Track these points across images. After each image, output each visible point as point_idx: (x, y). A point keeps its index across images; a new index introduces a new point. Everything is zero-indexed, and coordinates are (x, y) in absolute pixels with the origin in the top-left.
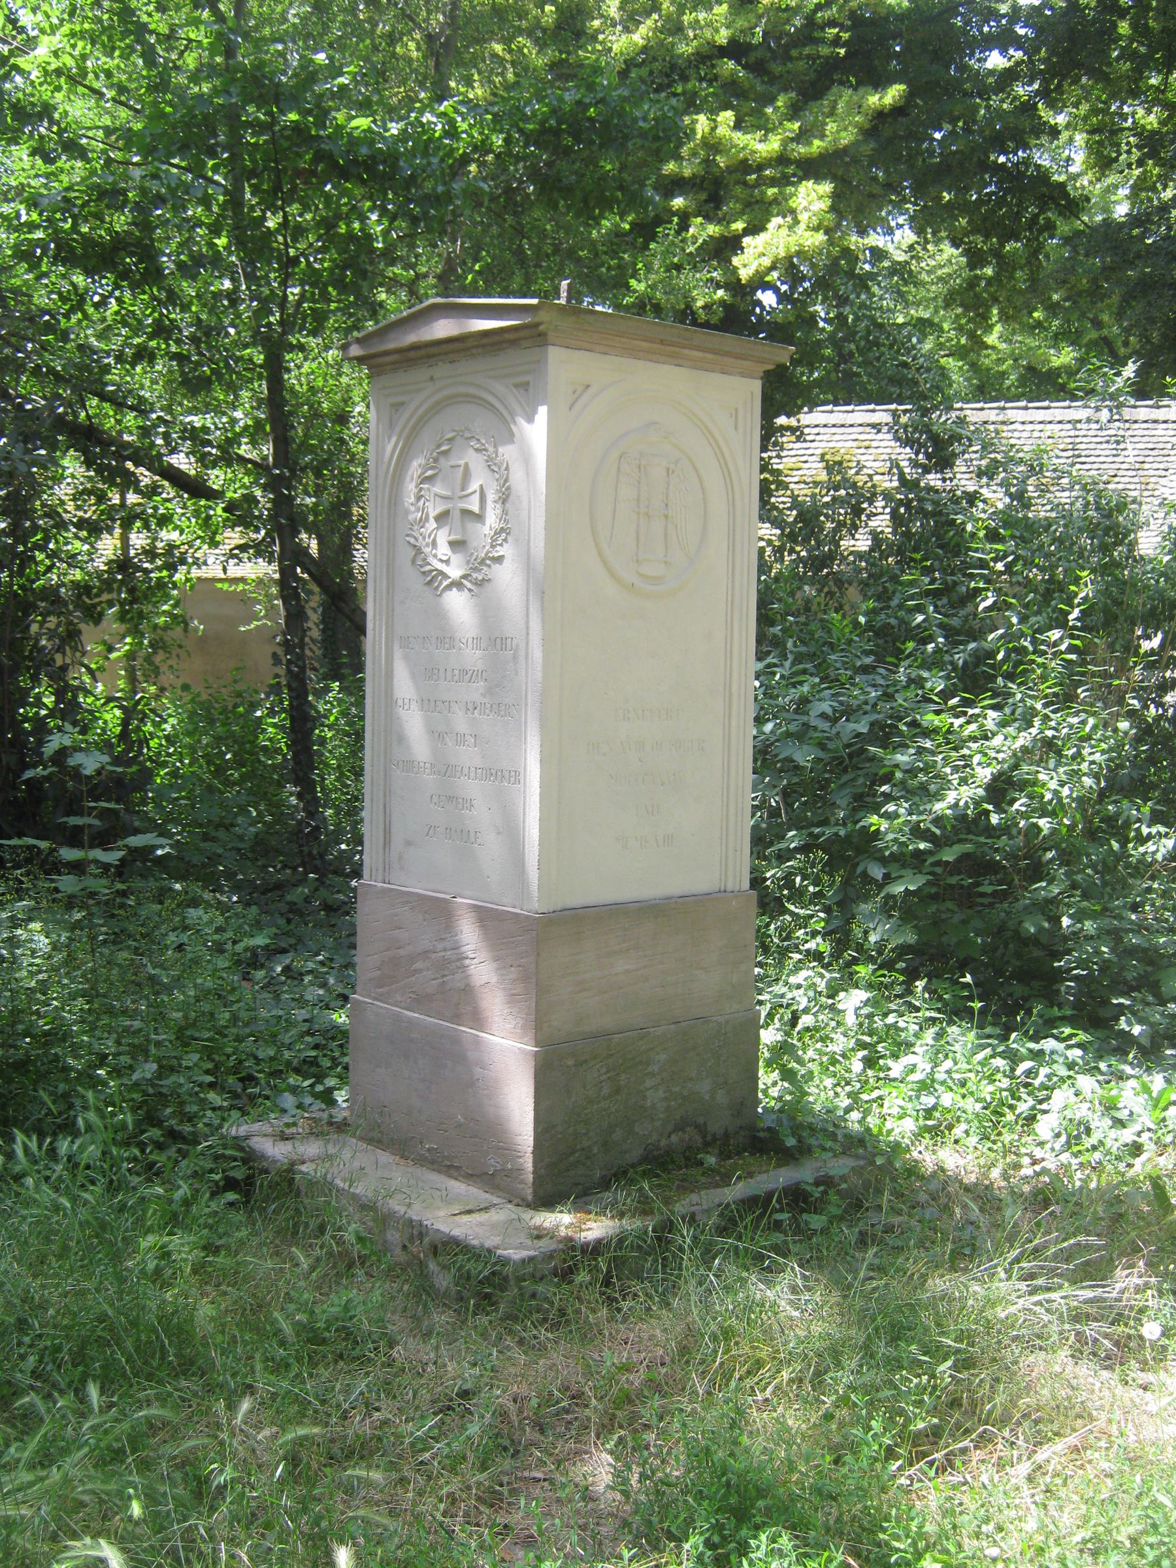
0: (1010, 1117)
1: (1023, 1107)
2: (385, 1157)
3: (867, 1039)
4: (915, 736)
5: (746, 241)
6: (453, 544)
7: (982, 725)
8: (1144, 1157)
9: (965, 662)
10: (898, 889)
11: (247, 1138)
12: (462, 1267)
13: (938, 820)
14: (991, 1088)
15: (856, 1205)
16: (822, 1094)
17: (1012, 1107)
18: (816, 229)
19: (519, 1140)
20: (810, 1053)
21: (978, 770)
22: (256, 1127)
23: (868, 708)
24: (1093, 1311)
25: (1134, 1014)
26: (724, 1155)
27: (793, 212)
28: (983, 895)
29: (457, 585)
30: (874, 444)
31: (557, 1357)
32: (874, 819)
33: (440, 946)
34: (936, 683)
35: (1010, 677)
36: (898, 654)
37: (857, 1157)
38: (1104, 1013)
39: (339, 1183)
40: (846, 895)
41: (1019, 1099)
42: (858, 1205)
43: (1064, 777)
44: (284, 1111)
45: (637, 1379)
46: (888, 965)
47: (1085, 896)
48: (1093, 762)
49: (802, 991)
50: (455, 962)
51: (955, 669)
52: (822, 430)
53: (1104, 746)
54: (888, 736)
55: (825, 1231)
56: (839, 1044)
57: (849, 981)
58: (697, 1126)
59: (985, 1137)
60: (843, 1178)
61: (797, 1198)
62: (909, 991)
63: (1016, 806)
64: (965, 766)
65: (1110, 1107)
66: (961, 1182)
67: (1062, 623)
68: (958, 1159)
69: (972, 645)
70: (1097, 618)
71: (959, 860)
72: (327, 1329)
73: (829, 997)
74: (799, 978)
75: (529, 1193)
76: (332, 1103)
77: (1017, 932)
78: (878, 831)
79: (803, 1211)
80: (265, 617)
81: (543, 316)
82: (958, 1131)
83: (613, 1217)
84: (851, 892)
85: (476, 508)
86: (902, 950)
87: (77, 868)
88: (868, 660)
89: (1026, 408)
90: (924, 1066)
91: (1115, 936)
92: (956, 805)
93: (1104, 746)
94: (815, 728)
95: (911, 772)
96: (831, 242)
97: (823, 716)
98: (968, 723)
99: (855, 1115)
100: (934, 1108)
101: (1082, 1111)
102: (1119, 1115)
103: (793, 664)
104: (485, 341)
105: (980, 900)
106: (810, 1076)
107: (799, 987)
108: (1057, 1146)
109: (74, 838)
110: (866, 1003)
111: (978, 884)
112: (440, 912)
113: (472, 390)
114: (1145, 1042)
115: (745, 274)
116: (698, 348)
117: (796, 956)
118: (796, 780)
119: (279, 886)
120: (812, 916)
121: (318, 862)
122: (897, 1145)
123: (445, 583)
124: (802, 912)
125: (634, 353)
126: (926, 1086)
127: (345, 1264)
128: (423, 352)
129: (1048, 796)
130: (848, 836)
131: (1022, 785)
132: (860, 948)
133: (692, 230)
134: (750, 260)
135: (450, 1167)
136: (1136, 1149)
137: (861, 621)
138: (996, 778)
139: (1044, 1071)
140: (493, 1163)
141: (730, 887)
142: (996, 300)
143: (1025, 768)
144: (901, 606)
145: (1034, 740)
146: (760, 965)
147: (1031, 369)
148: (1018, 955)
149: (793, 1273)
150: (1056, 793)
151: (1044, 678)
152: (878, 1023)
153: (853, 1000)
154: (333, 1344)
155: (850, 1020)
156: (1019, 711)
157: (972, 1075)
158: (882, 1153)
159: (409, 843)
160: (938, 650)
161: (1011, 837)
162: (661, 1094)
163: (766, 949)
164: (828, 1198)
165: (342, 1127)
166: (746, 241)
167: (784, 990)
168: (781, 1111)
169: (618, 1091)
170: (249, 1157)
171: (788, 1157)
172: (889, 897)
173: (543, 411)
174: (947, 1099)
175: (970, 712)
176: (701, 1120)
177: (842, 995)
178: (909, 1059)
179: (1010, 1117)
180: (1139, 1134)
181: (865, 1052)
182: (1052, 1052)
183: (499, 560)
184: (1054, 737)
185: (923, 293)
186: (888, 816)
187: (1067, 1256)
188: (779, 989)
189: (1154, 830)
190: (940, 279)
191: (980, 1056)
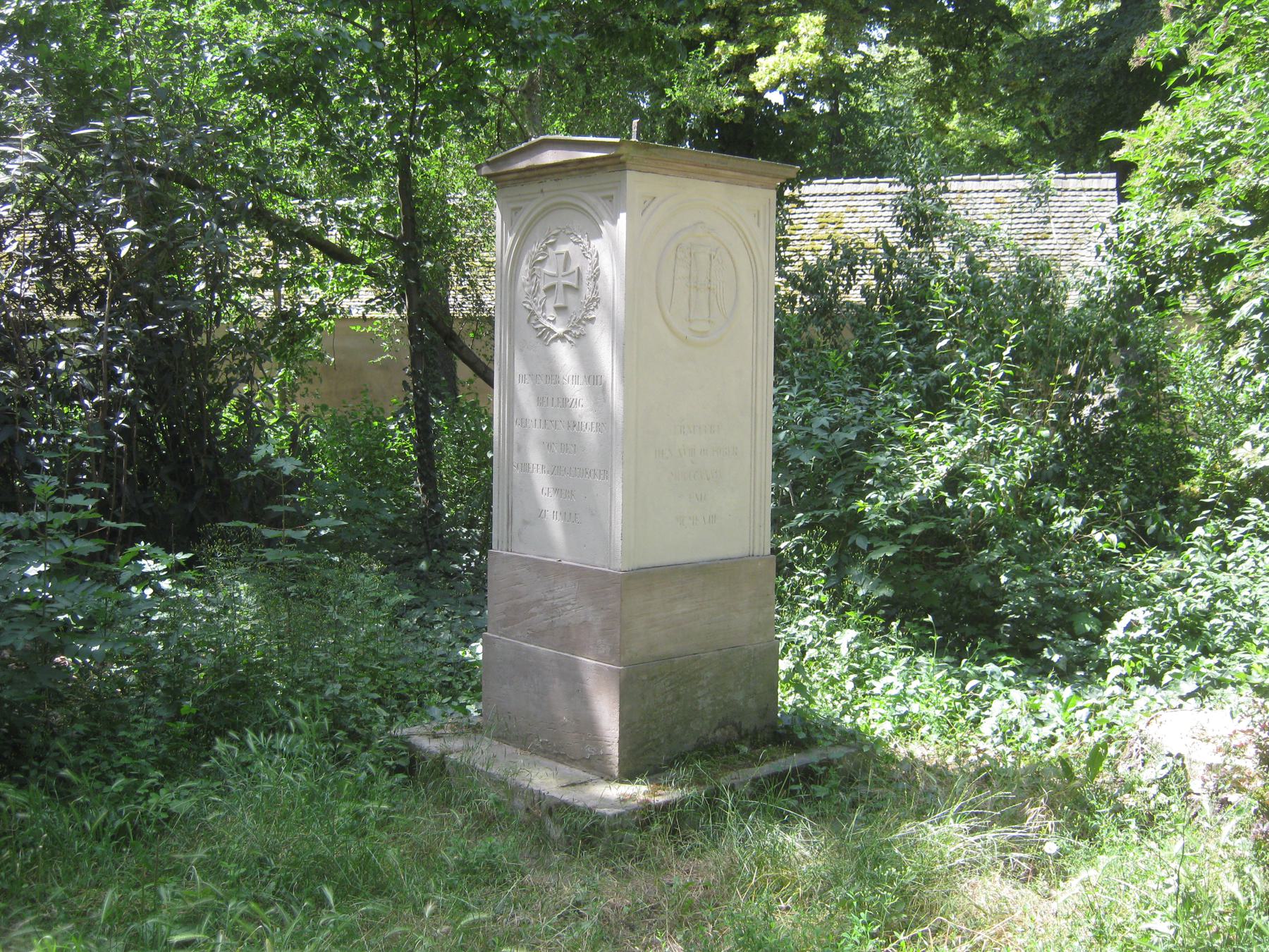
0: (962, 721)
1: (971, 714)
2: (510, 749)
3: (857, 666)
4: (891, 442)
5: (760, 61)
6: (558, 309)
7: (940, 434)
8: (1057, 746)
9: (928, 387)
10: (877, 556)
11: (408, 736)
12: (570, 822)
13: (908, 504)
14: (948, 699)
15: (849, 780)
16: (824, 705)
17: (963, 714)
18: (813, 50)
19: (608, 733)
20: (815, 676)
21: (937, 467)
22: (414, 729)
23: (856, 422)
24: (1013, 845)
25: (1054, 646)
26: (754, 746)
27: (795, 36)
28: (943, 560)
29: (561, 338)
30: (860, 209)
31: (640, 881)
32: (861, 503)
33: (549, 596)
34: (906, 402)
35: (961, 397)
36: (878, 382)
37: (850, 747)
38: (1032, 646)
39: (479, 766)
40: (840, 561)
41: (968, 708)
42: (851, 781)
43: (1001, 472)
44: (433, 719)
45: (696, 895)
46: (872, 611)
47: (1018, 560)
48: (1022, 461)
49: (808, 631)
51: (920, 390)
52: (818, 198)
53: (1031, 448)
54: (871, 442)
55: (827, 798)
56: (836, 669)
57: (843, 623)
58: (734, 725)
59: (943, 734)
60: (840, 761)
61: (807, 775)
62: (887, 631)
63: (965, 493)
64: (928, 464)
65: (1033, 711)
66: (924, 764)
67: (998, 358)
68: (924, 749)
69: (934, 373)
70: (1026, 353)
71: (922, 534)
72: (477, 864)
73: (828, 635)
74: (807, 621)
75: (616, 771)
76: (467, 713)
77: (968, 588)
78: (863, 512)
79: (812, 783)
80: (389, 352)
81: (623, 150)
82: (924, 730)
83: (676, 788)
84: (844, 558)
85: (574, 284)
86: (883, 600)
87: (270, 543)
88: (856, 387)
89: (980, 180)
90: (898, 684)
91: (1040, 589)
92: (920, 494)
93: (1031, 448)
94: (817, 437)
95: (889, 468)
96: (826, 60)
97: (822, 427)
98: (930, 432)
99: (847, 719)
100: (906, 713)
101: (1014, 715)
102: (1040, 717)
103: (800, 389)
104: (582, 166)
105: (939, 563)
106: (815, 692)
107: (806, 628)
108: (996, 740)
109: (275, 523)
110: (856, 639)
111: (939, 552)
113: (570, 200)
114: (1062, 667)
115: (759, 86)
116: (731, 170)
117: (804, 605)
118: (802, 475)
119: (408, 559)
120: (815, 576)
121: (437, 540)
122: (879, 741)
124: (807, 572)
125: (686, 174)
126: (901, 698)
127: (485, 822)
128: (536, 172)
129: (989, 486)
130: (841, 517)
131: (967, 479)
132: (850, 599)
133: (717, 50)
134: (765, 72)
135: (557, 755)
136: (1052, 741)
137: (849, 355)
138: (950, 473)
139: (986, 687)
141: (756, 553)
142: (955, 95)
143: (971, 465)
144: (880, 344)
145: (978, 444)
146: (778, 612)
147: (984, 147)
148: (969, 605)
149: (804, 825)
150: (994, 483)
151: (985, 398)
152: (865, 654)
153: (846, 637)
154: (483, 875)
155: (844, 651)
156: (968, 423)
157: (933, 690)
158: (867, 743)
159: (525, 523)
160: (907, 378)
161: (963, 517)
162: (709, 700)
163: (781, 601)
164: (832, 776)
165: (477, 729)
166: (760, 61)
167: (795, 631)
168: (794, 714)
169: (678, 698)
170: (412, 748)
171: (800, 746)
172: (871, 561)
173: (623, 216)
174: (915, 707)
175: (931, 424)
176: (737, 721)
177: (838, 633)
178: (886, 679)
179: (962, 721)
180: (1054, 730)
181: (855, 676)
182: (992, 673)
183: (592, 320)
184: (994, 442)
185: (897, 87)
186: (871, 501)
187: (995, 805)
188: (791, 629)
189: (1067, 511)
190: (911, 76)
191: (939, 675)
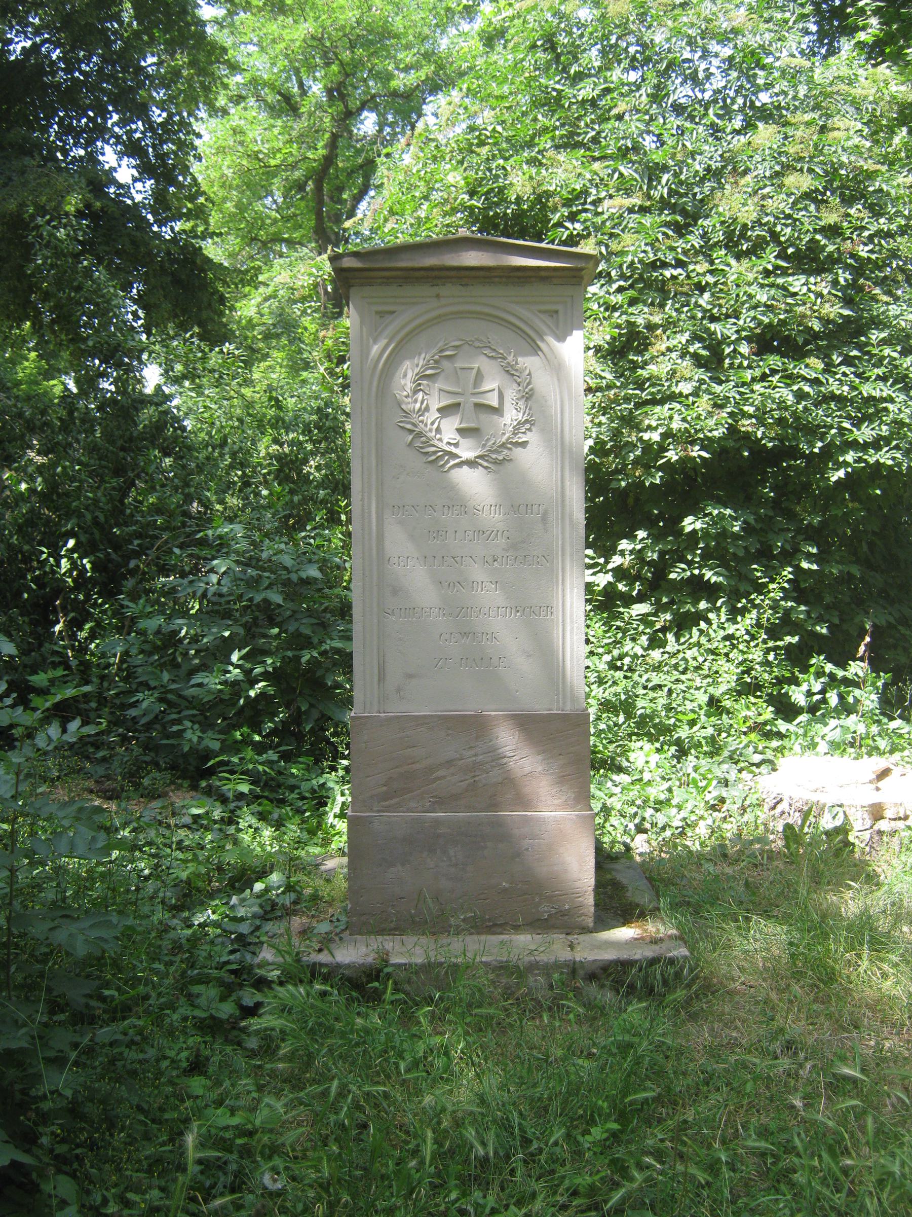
50: (496, 759)
85: (495, 403)
112: (475, 727)
123: (452, 463)
128: (436, 273)
140: (545, 910)
183: (524, 444)
